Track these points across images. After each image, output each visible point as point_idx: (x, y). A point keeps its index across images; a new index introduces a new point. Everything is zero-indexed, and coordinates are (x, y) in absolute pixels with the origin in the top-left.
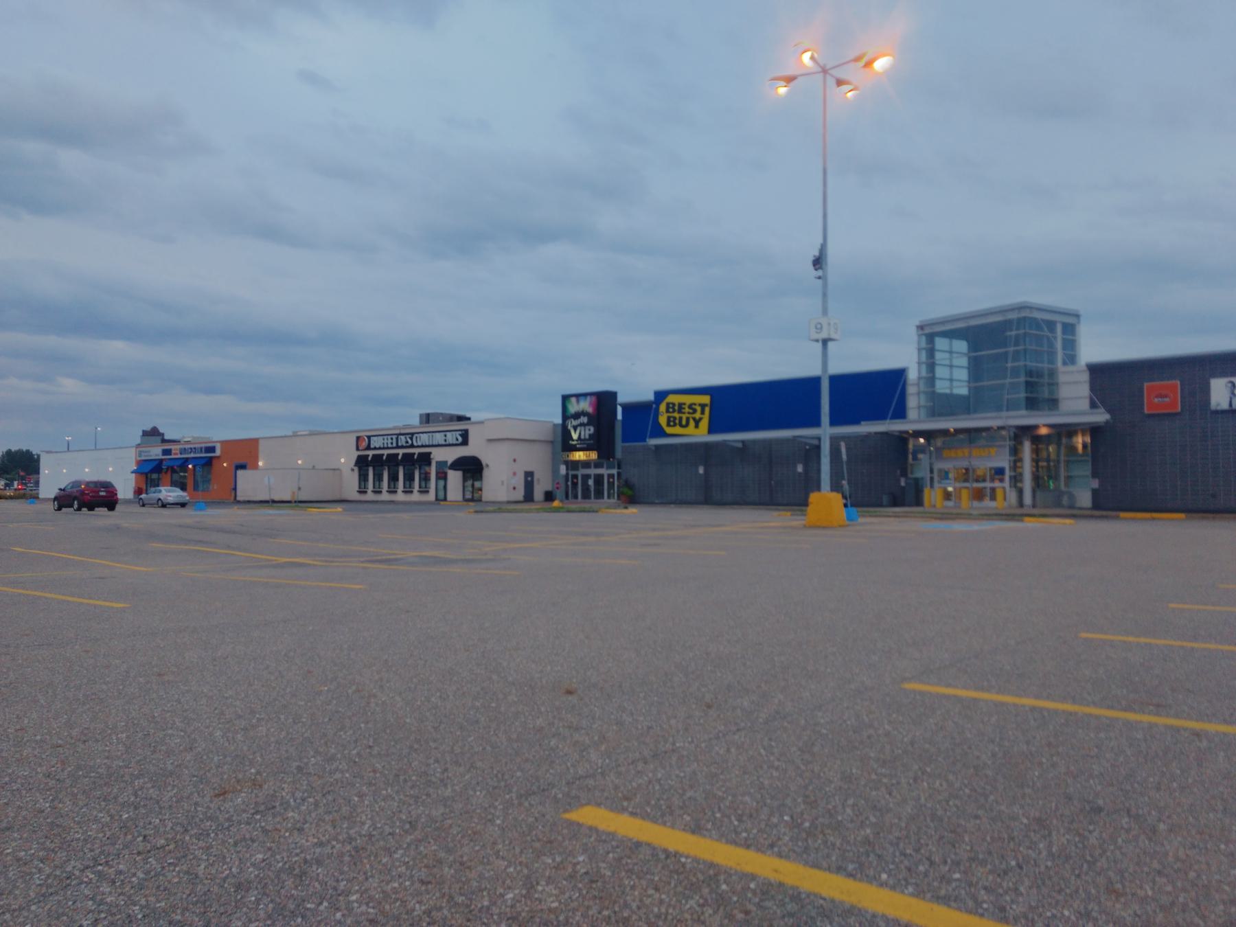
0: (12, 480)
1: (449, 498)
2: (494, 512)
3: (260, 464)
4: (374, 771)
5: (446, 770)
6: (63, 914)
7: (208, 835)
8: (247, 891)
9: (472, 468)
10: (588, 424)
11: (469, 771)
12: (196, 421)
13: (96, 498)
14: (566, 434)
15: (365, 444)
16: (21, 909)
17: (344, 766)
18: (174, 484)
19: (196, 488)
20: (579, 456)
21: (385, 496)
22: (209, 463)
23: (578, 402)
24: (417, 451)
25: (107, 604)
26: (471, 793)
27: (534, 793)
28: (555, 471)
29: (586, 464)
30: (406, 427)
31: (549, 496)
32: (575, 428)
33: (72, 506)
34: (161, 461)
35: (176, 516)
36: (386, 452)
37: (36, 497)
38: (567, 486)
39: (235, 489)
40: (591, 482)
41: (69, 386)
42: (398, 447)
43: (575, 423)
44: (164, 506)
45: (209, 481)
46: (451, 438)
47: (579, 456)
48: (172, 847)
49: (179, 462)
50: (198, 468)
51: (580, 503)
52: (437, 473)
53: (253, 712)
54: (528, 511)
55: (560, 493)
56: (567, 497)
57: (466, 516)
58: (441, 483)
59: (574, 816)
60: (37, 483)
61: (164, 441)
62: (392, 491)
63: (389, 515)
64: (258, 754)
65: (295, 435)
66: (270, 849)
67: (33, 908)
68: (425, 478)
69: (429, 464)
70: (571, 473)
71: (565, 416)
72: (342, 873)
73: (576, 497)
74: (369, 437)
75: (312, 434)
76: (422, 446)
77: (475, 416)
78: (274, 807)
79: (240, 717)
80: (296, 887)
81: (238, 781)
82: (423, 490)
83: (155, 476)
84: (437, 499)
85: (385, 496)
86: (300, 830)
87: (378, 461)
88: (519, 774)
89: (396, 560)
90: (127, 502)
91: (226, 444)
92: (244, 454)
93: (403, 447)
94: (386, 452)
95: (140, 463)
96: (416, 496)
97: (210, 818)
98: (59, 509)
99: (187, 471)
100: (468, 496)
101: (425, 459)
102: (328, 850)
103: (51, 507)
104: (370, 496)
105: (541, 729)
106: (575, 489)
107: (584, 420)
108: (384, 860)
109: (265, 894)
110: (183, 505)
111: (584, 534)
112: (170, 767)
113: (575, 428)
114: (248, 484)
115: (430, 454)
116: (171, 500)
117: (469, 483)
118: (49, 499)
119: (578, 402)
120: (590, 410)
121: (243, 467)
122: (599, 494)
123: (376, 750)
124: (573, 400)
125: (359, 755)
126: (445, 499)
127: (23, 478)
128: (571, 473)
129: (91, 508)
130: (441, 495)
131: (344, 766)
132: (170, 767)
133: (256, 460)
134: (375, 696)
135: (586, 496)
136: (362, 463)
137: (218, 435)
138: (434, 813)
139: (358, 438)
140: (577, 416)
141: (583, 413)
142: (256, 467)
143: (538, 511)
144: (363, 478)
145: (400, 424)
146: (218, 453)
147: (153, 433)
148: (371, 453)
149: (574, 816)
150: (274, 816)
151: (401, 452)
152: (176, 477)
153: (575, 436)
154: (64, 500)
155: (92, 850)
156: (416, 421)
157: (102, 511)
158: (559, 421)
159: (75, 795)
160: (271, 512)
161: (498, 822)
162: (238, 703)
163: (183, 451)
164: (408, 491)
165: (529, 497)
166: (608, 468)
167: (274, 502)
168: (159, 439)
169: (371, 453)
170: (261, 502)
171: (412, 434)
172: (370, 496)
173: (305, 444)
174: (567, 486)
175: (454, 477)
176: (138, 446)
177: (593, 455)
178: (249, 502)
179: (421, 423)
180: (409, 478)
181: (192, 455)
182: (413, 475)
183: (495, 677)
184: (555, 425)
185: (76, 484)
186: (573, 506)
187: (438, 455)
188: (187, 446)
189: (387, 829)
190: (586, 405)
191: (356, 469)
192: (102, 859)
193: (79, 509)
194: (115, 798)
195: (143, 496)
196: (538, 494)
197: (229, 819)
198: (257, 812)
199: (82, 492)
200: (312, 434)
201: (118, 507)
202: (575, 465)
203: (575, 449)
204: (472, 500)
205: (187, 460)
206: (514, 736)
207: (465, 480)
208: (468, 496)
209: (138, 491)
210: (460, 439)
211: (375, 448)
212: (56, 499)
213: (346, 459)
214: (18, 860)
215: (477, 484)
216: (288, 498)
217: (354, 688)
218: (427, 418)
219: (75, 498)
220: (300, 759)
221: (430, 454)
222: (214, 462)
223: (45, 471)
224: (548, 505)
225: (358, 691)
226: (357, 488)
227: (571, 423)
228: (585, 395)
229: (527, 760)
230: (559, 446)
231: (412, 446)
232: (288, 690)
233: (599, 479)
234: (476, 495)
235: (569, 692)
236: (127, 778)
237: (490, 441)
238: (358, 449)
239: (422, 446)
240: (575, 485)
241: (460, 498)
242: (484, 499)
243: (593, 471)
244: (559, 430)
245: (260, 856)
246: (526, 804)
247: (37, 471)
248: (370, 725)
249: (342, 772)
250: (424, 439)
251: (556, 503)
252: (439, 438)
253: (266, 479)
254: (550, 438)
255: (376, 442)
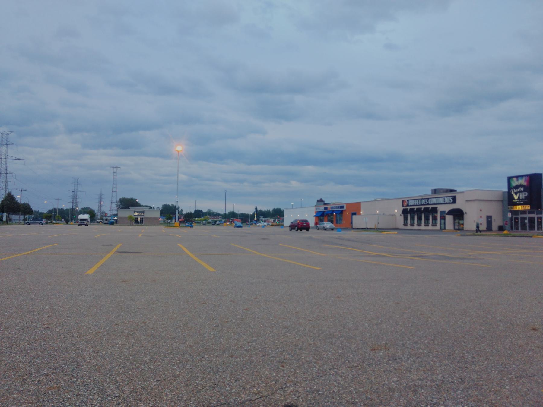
0: (275, 219)
1: (447, 228)
2: (471, 235)
3: (361, 213)
4: (437, 351)
5: (474, 357)
6: (327, 385)
7: (372, 366)
8: (394, 392)
9: (458, 214)
10: (524, 191)
11: (486, 360)
12: (337, 195)
13: (301, 226)
14: (510, 197)
15: (406, 204)
16: (311, 380)
17: (422, 347)
18: (329, 221)
19: (337, 222)
20: (519, 208)
21: (416, 227)
22: (341, 212)
23: (517, 180)
24: (430, 206)
25: (285, 260)
26: (490, 371)
27: (524, 377)
28: (504, 216)
29: (523, 212)
30: (425, 195)
31: (501, 228)
32: (516, 193)
33: (295, 229)
34: (324, 212)
35: (329, 234)
36: (416, 207)
37: (283, 225)
38: (512, 223)
39: (352, 223)
40: (526, 221)
41: (294, 184)
42: (421, 205)
43: (516, 191)
44: (325, 229)
45: (341, 220)
46: (447, 200)
47: (519, 208)
48: (360, 367)
49: (330, 212)
50: (338, 215)
51: (520, 232)
52: (441, 217)
53: (378, 317)
54: (489, 235)
55: (508, 227)
56: (512, 229)
57: (456, 236)
58: (443, 221)
59: (214, 270)
60: (283, 220)
61: (325, 204)
62: (419, 225)
63: (419, 236)
64: (384, 336)
65: (375, 200)
66: (399, 377)
67: (316, 380)
68: (435, 219)
69: (437, 212)
70: (514, 216)
71: (510, 187)
72: (434, 395)
73: (517, 229)
74: (408, 201)
75: (383, 200)
76: (433, 204)
77: (459, 190)
78: (396, 359)
79: (373, 319)
80: (414, 396)
81: (379, 346)
82: (434, 225)
83: (322, 218)
84: (441, 229)
85: (416, 227)
86: (410, 371)
87: (412, 211)
88: (514, 366)
89: (426, 256)
90: (313, 228)
91: (348, 204)
92: (355, 209)
93: (424, 205)
94: (416, 207)
95: (317, 213)
96: (430, 227)
97: (371, 359)
98: (291, 230)
99: (334, 216)
100: (457, 227)
101: (435, 210)
102: (424, 383)
103: (288, 229)
104: (409, 227)
105: (521, 346)
106: (516, 225)
107: (522, 189)
108: (452, 394)
109: (401, 395)
110: (332, 229)
111: (525, 249)
112: (351, 335)
113: (516, 193)
114: (357, 221)
115: (436, 208)
116: (328, 227)
117: (457, 221)
118: (287, 226)
119: (517, 180)
120: (525, 184)
121: (355, 214)
122: (532, 227)
123: (436, 342)
124: (515, 179)
125: (428, 343)
126: (445, 229)
127: (279, 218)
128: (514, 216)
129: (301, 230)
130: (443, 226)
131: (422, 347)
132: (351, 335)
133: (360, 211)
134: (430, 317)
135: (524, 228)
136: (405, 212)
137: (344, 201)
138: (472, 376)
139: (403, 201)
140: (517, 187)
141: (521, 186)
142: (360, 214)
143: (495, 235)
144: (406, 219)
145: (422, 194)
146: (345, 208)
147: (320, 201)
148: (409, 208)
149: (214, 270)
150: (397, 363)
151: (423, 207)
152: (329, 218)
153: (516, 197)
154: (293, 227)
155: (331, 363)
156: (430, 193)
157: (304, 231)
158: (506, 190)
159: (320, 340)
160: (367, 233)
161: (507, 387)
162: (371, 313)
163: (332, 208)
164: (427, 225)
165: (489, 228)
166: (537, 214)
167: (368, 229)
168: (323, 203)
169: (409, 208)
170: (362, 229)
171: (428, 199)
172: (409, 227)
173: (381, 207)
174: (512, 223)
175: (449, 219)
176: (316, 206)
177: (528, 207)
178: (358, 229)
179: (432, 193)
180: (427, 219)
181: (335, 209)
182: (429, 217)
183: (489, 316)
184: (504, 193)
185: (296, 221)
186: (516, 234)
187: (441, 208)
188: (333, 206)
189: (450, 380)
190: (522, 181)
191: (402, 215)
192: (335, 367)
193: (297, 230)
194: (335, 344)
195: (318, 226)
196: (495, 227)
197: (379, 361)
198: (390, 360)
199: (298, 224)
200: (383, 200)
201: (310, 230)
202: (516, 212)
203: (516, 204)
204: (459, 229)
205: (333, 212)
206: (507, 347)
207: (454, 220)
208: (457, 227)
209: (316, 224)
210: (452, 200)
211: (411, 206)
212: (290, 226)
213: (398, 211)
214: (307, 361)
215: (461, 222)
216: (373, 227)
217: (419, 312)
218: (435, 191)
219: (296, 226)
220: (403, 341)
221: (436, 208)
222: (344, 212)
223: (285, 216)
224: (500, 233)
225: (421, 314)
226: (403, 223)
227: (513, 192)
228: (522, 176)
229: (517, 360)
230: (506, 203)
231: (428, 204)
232: (391, 310)
233: (531, 220)
234: (460, 227)
235: (534, 329)
236: (337, 337)
237: (467, 201)
238: (403, 206)
239: (433, 204)
240: (516, 223)
241: (452, 228)
242: (465, 229)
243: (528, 216)
244: (507, 195)
245: (395, 379)
246: (521, 381)
247: (283, 216)
248: (431, 330)
249: (422, 349)
250: (434, 201)
251: (506, 232)
252: (441, 200)
253: (364, 219)
254: (501, 199)
255: (411, 203)
